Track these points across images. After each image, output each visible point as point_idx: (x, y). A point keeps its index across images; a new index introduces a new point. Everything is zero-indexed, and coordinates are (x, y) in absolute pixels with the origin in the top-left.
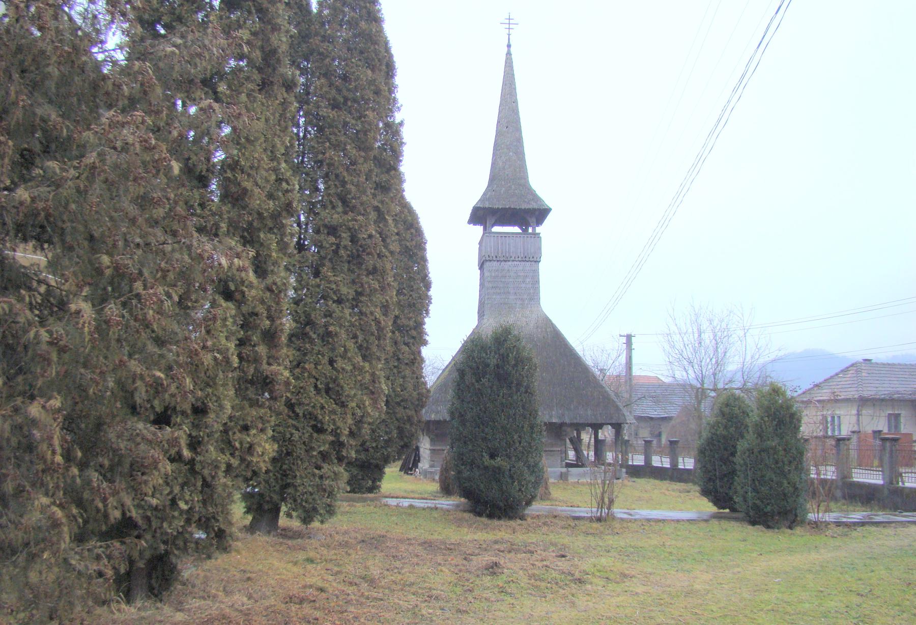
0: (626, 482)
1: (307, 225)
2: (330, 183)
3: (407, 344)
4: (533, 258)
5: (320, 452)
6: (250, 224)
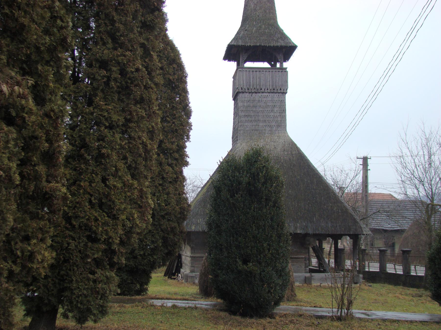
0: (363, 286)
1: (80, 59)
2: (100, 21)
3: (169, 165)
4: (282, 90)
5: (94, 259)
6: (28, 56)
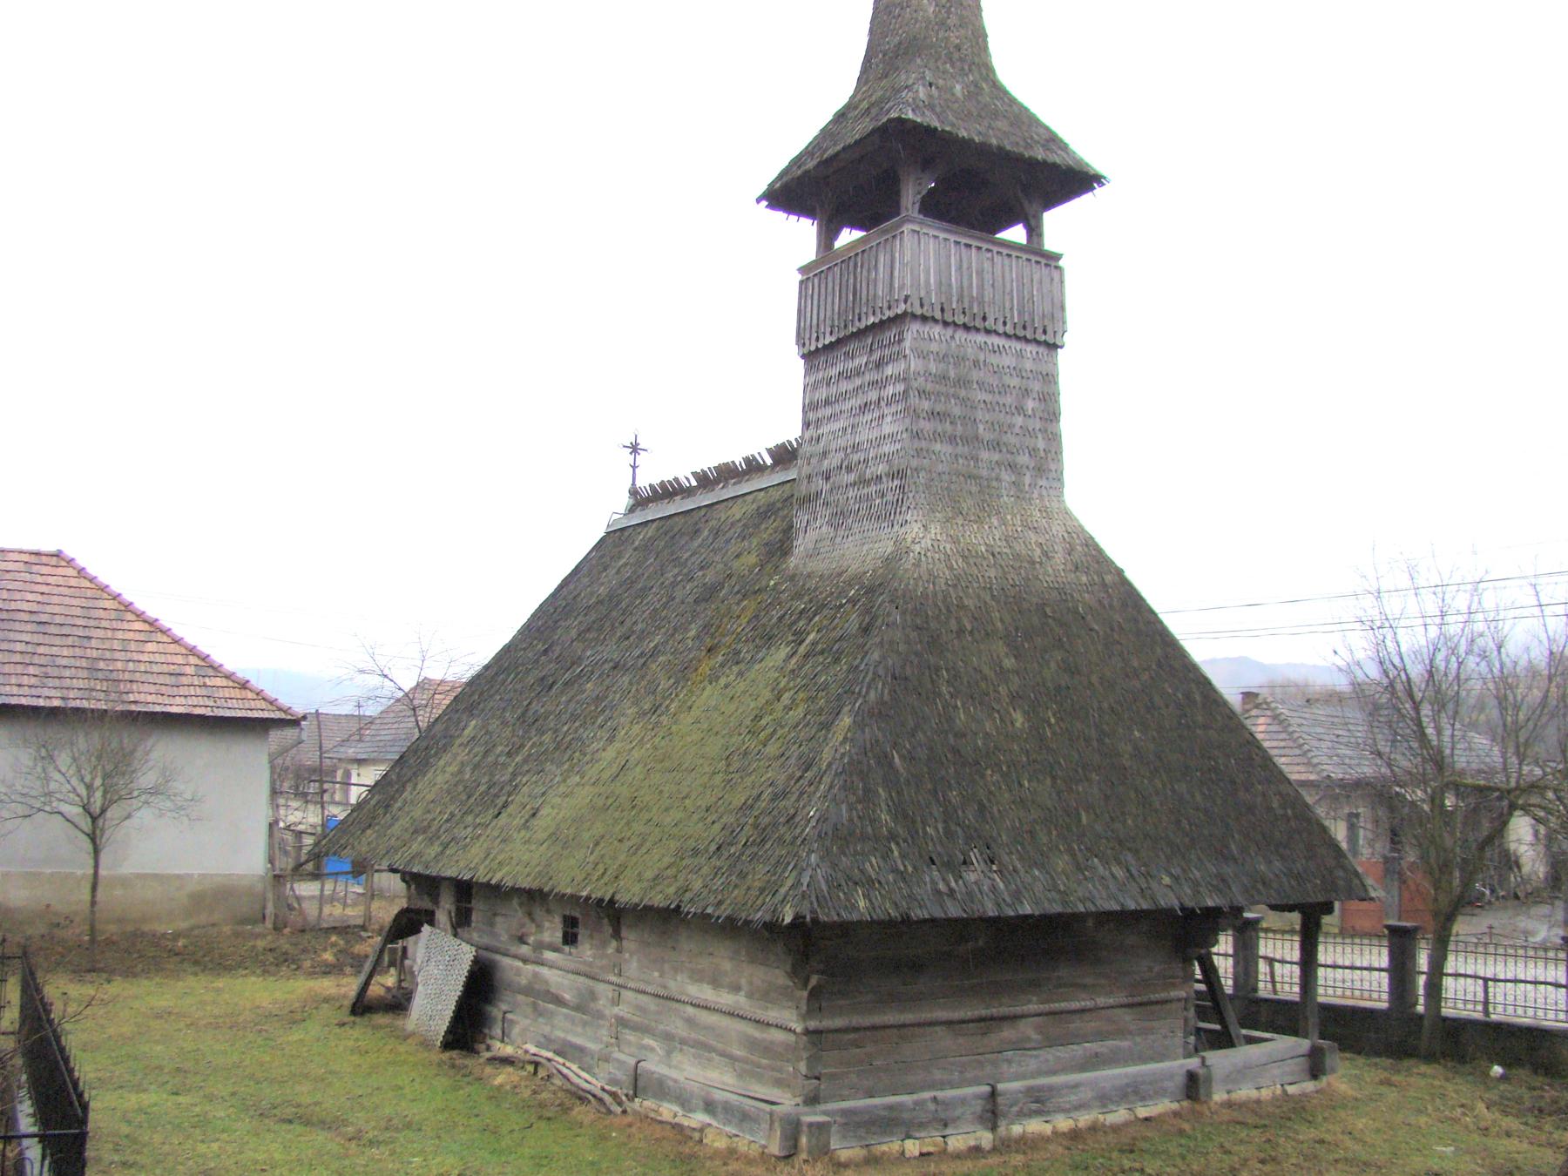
4: (1043, 334)
